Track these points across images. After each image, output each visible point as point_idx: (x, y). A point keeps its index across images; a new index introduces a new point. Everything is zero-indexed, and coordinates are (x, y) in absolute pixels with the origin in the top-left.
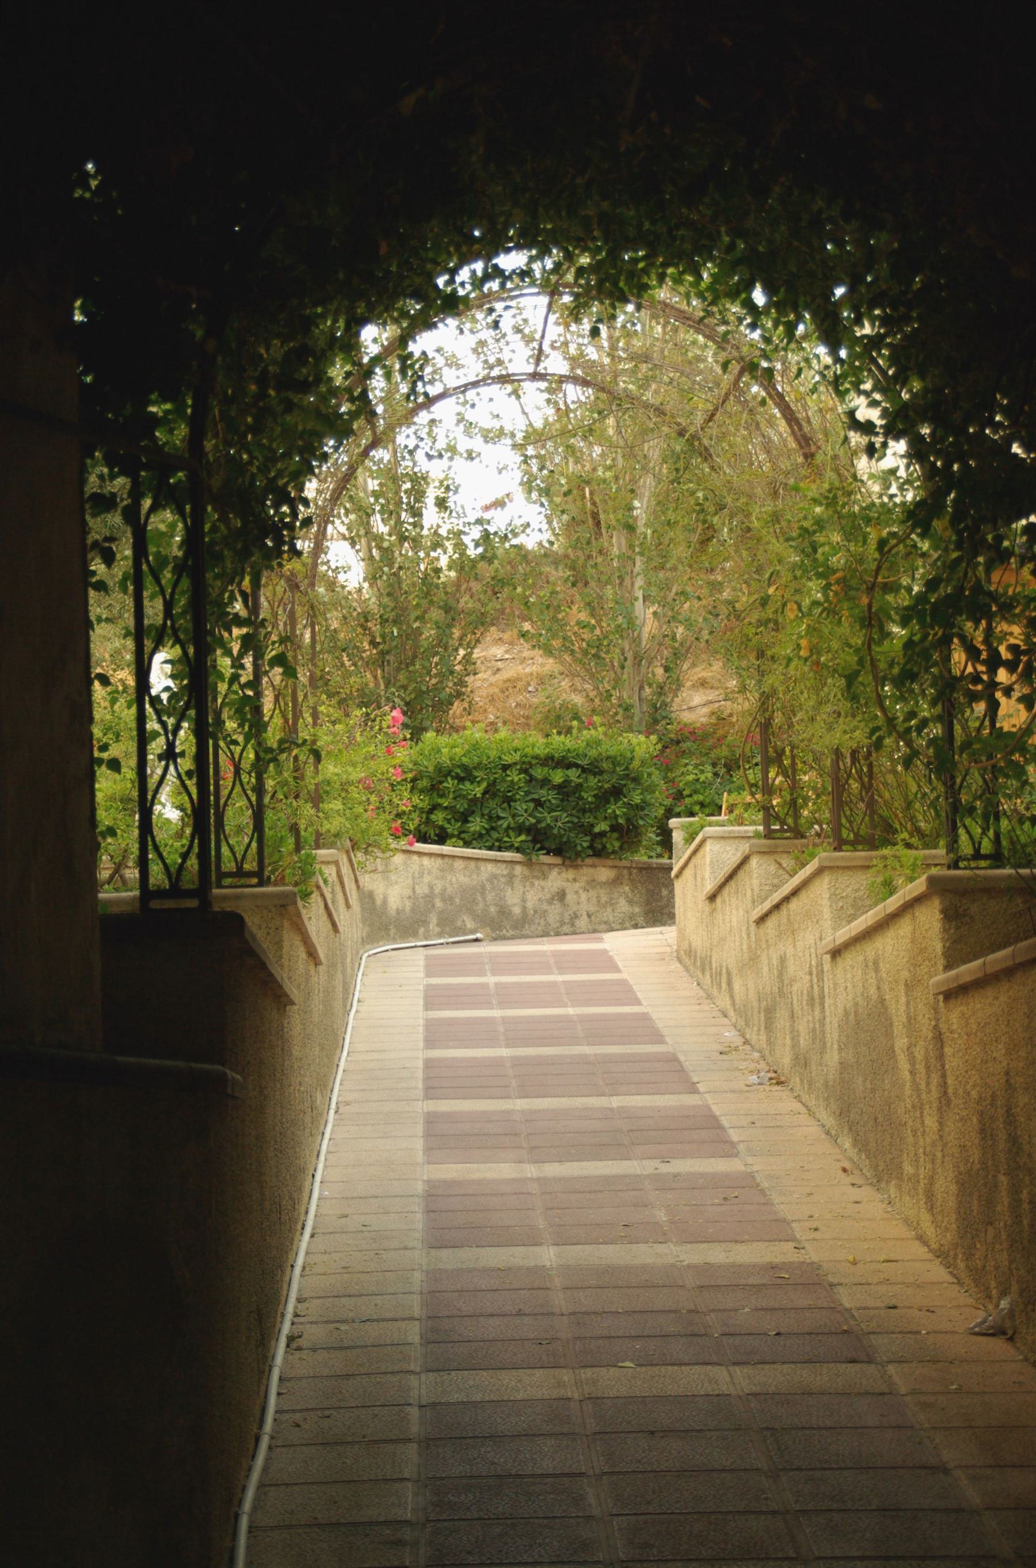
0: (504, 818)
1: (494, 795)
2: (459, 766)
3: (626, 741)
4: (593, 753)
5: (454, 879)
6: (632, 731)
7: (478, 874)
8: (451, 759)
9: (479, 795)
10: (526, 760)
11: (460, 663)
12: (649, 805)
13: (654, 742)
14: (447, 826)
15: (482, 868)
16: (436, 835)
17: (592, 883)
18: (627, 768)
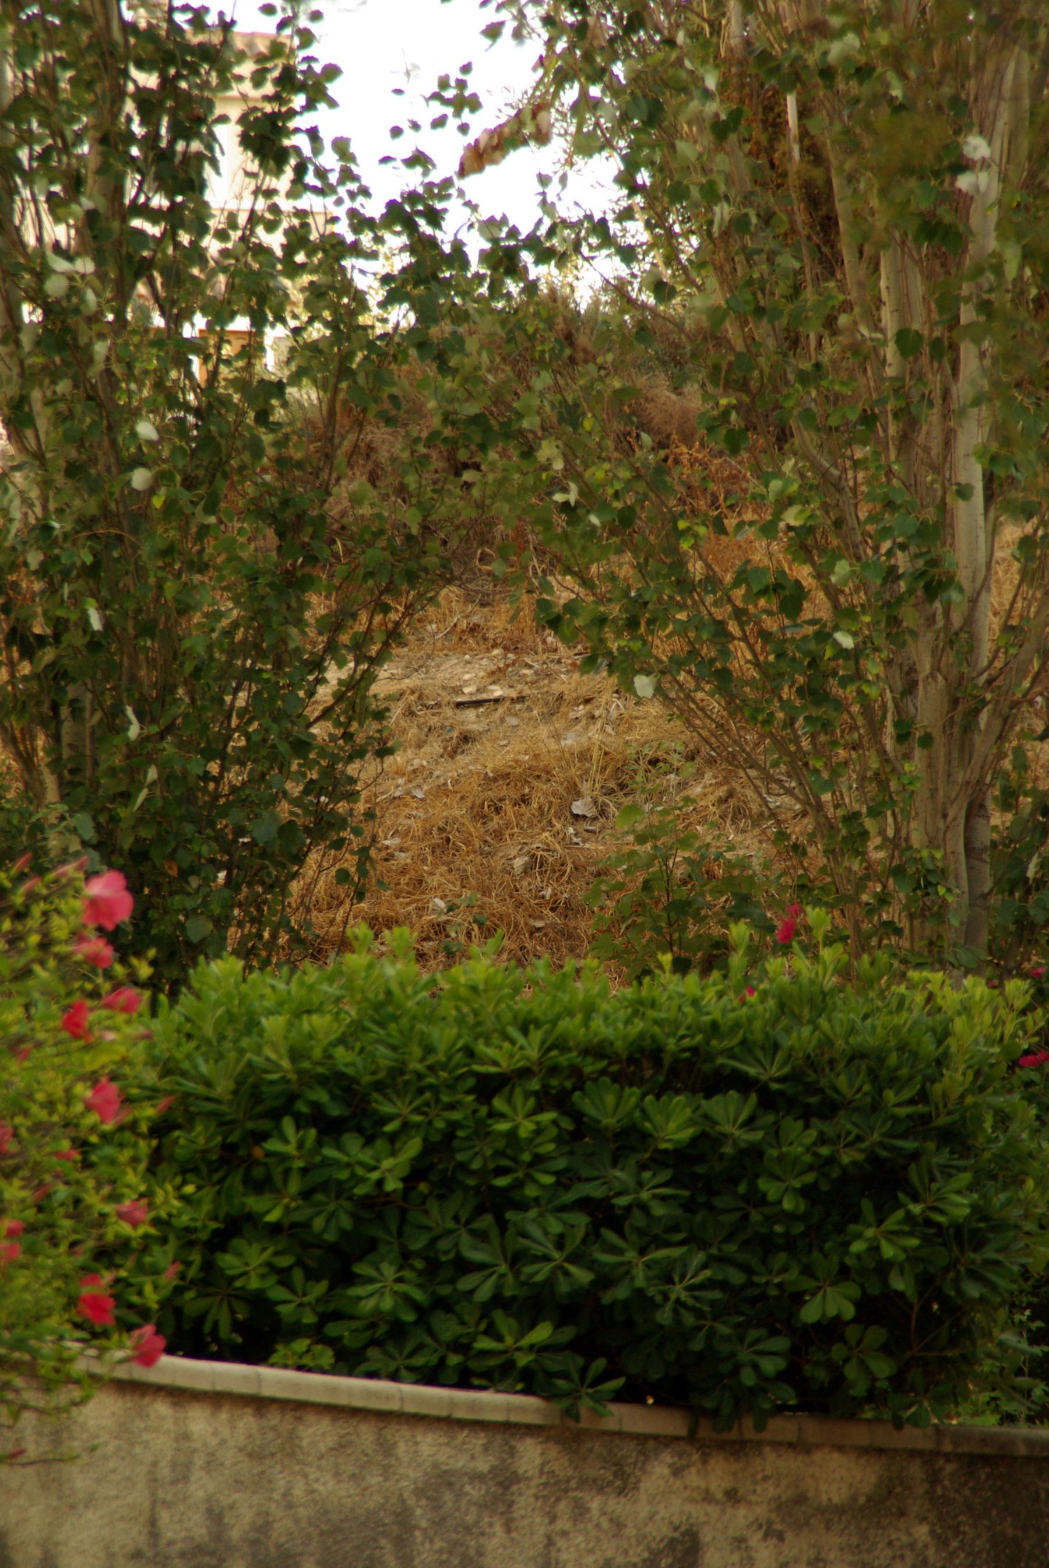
0: (480, 1267)
1: (447, 1186)
2: (322, 1081)
3: (920, 998)
4: (801, 1038)
5: (299, 1490)
6: (942, 964)
7: (387, 1472)
8: (296, 1055)
9: (392, 1185)
10: (563, 1060)
11: (326, 713)
12: (1000, 1226)
13: (1020, 1003)
14: (278, 1293)
15: (401, 1449)
16: (237, 1326)
17: (795, 1511)
18: (923, 1096)
